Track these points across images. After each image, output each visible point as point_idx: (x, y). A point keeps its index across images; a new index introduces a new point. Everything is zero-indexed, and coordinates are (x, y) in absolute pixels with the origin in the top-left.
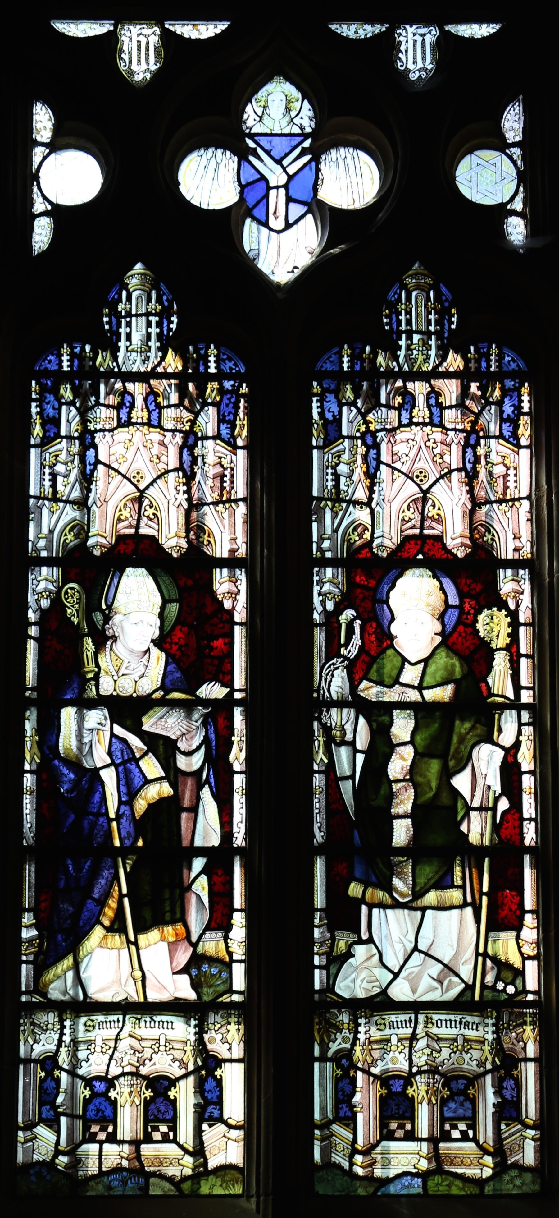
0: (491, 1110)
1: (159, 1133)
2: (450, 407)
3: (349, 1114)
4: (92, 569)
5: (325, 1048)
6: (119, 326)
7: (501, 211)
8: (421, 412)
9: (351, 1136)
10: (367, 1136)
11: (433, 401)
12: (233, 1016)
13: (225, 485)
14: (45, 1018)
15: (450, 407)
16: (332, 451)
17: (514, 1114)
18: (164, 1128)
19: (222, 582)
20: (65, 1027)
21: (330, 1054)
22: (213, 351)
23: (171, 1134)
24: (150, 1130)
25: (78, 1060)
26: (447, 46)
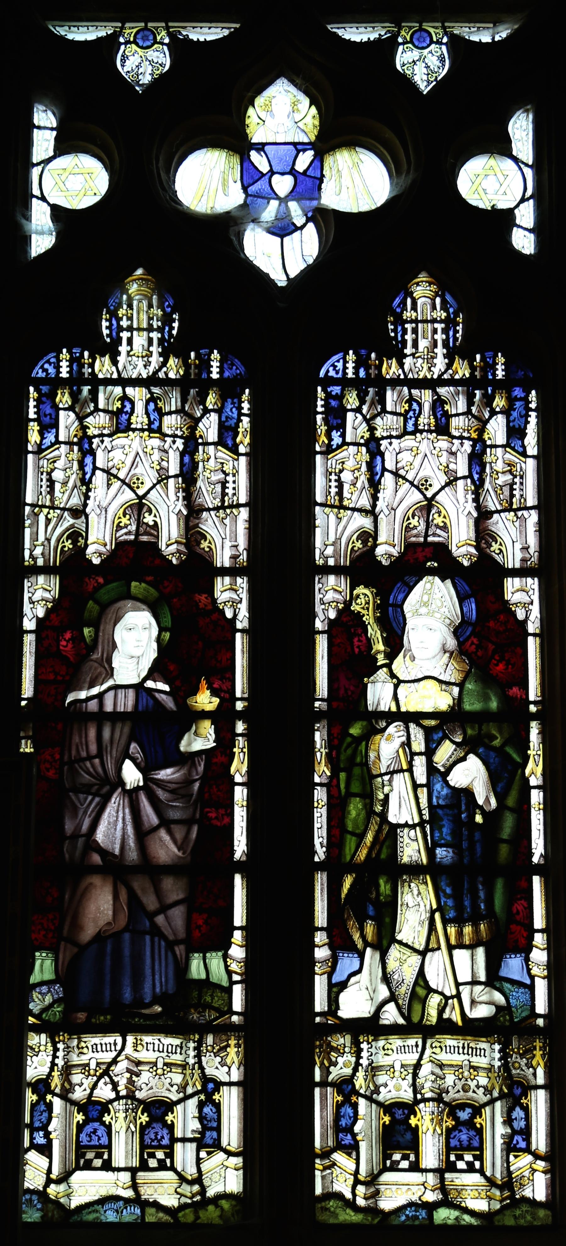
0: (499, 1141)
4: (388, 578)
5: (326, 1072)
6: (405, 332)
7: (504, 219)
8: (426, 419)
11: (152, 406)
12: (233, 1038)
13: (514, 492)
14: (342, 1041)
19: (223, 591)
23: (168, 1161)
24: (146, 1157)
25: (70, 1083)
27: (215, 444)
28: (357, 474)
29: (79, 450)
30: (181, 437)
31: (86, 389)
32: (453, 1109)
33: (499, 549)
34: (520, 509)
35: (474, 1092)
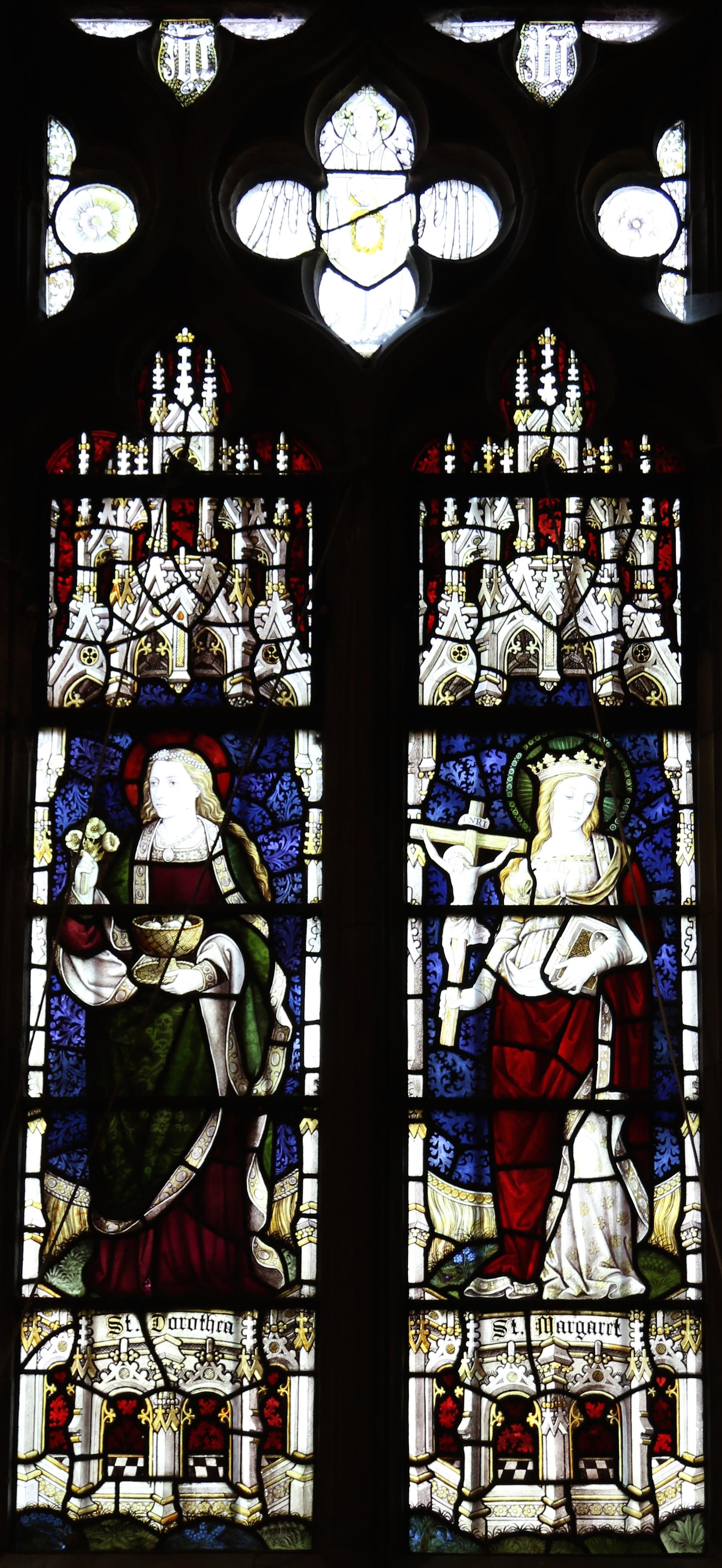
1: (517, 1471)
7: (653, 267)
9: (67, 1476)
17: (279, 1447)
18: (601, 1464)
32: (583, 1402)
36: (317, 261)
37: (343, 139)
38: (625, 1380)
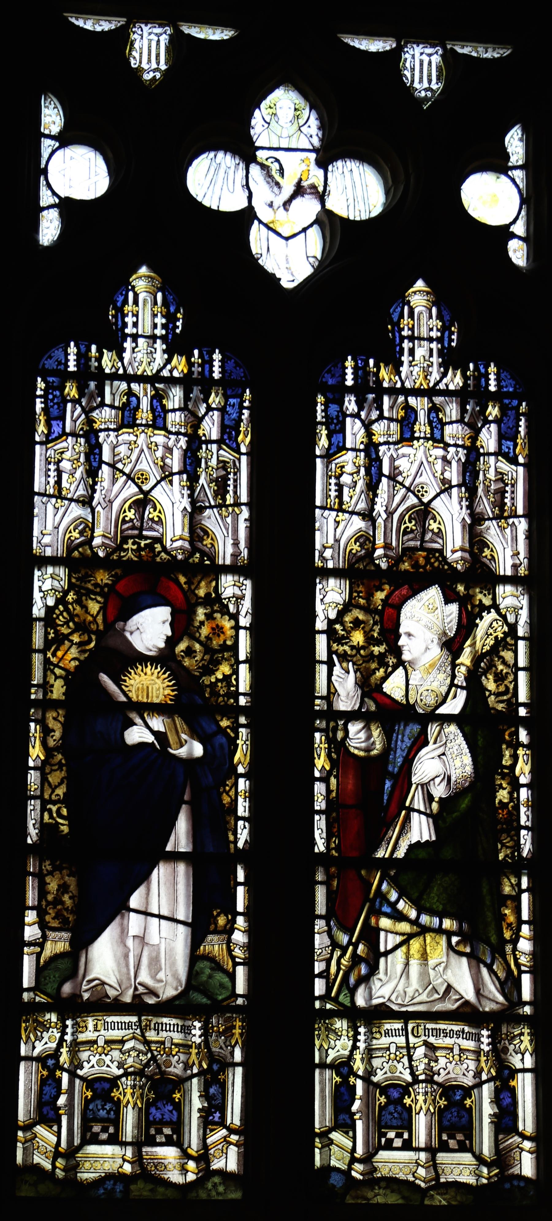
2: (174, 410)
3: (349, 1121)
7: (504, 233)
8: (144, 415)
10: (366, 1143)
15: (174, 410)
16: (55, 448)
20: (67, 1026)
21: (329, 1060)
22: (492, 369)
26: (179, 45)
27: (495, 454)
28: (356, 478)
29: (365, 456)
30: (185, 435)
31: (92, 385)
33: (491, 555)
34: (510, 517)
35: (108, 1066)
36: (247, 216)
37: (269, 124)
38: (187, 1066)
